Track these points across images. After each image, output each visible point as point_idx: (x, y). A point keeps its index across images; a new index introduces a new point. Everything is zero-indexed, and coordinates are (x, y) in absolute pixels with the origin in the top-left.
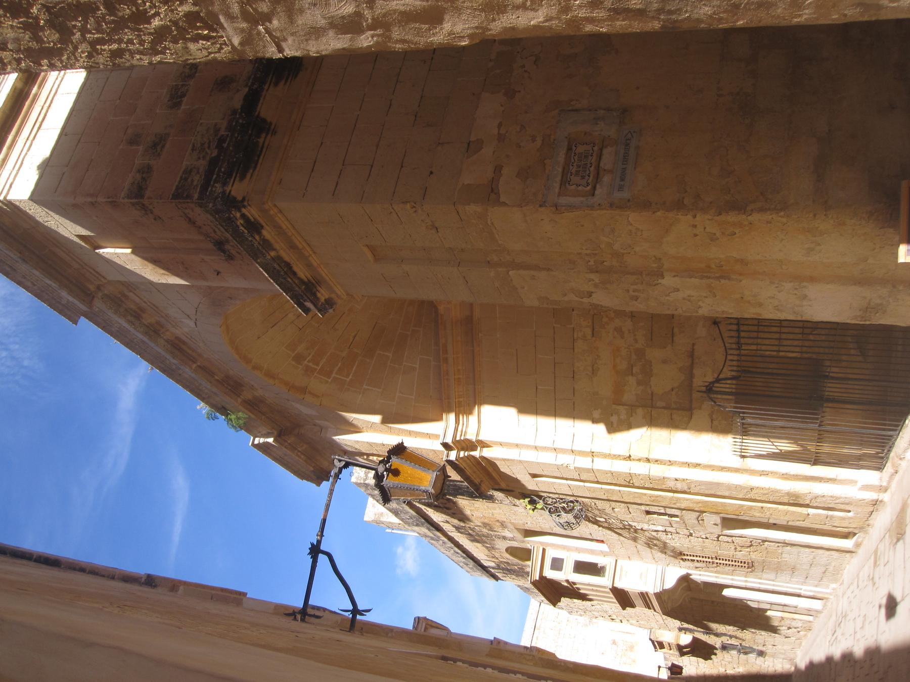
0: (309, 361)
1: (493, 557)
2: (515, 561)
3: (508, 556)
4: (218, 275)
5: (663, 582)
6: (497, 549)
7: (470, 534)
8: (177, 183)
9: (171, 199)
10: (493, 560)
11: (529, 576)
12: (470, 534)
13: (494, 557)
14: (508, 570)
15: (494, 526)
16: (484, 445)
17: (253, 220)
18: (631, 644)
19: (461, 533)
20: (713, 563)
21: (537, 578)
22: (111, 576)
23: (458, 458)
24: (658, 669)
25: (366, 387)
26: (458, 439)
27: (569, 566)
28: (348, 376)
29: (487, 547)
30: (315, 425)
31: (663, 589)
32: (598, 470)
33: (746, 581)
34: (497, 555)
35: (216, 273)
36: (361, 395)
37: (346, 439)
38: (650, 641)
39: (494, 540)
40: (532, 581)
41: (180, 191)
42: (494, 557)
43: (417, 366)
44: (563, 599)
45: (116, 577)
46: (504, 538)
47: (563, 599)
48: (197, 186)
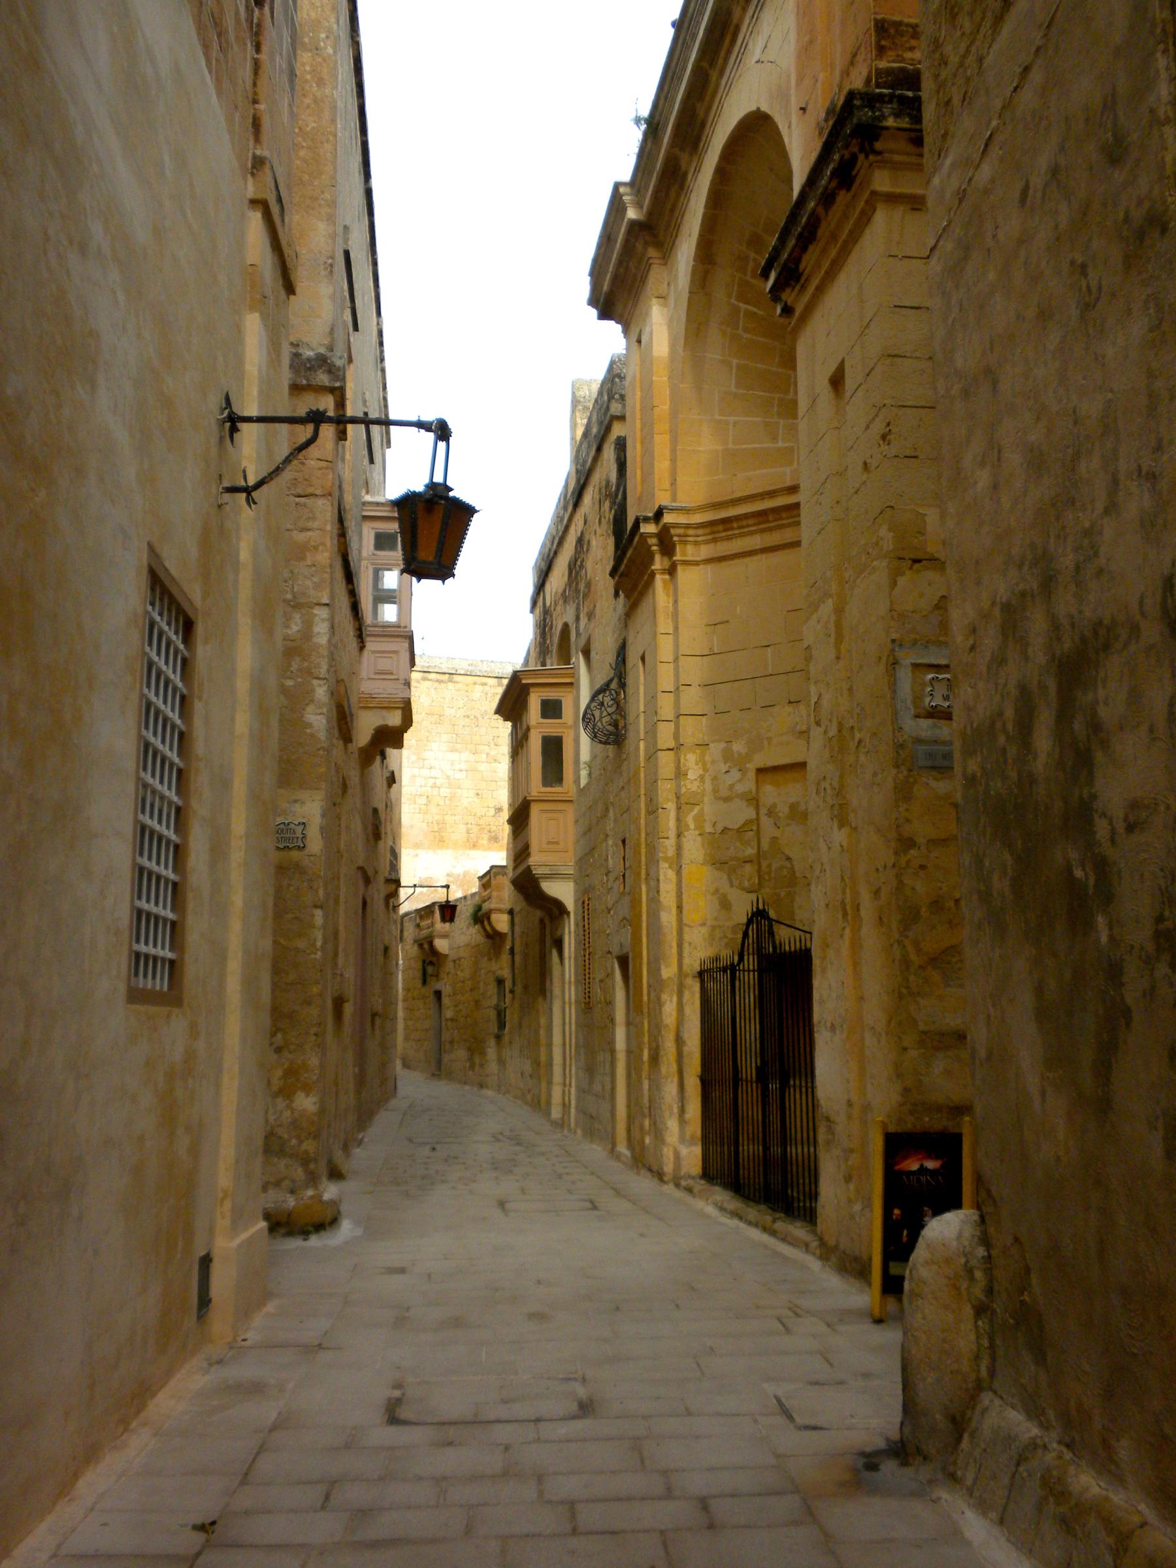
0: (755, 260)
1: (555, 602)
2: (556, 639)
3: (559, 627)
4: (802, 109)
5: (550, 877)
6: (565, 608)
7: (576, 560)
8: (906, 20)
9: (875, 19)
10: (553, 603)
11: (542, 666)
12: (576, 560)
13: (556, 605)
14: (544, 629)
15: (588, 600)
16: (671, 571)
17: (854, 173)
18: (501, 838)
19: (576, 548)
20: (585, 950)
21: (524, 682)
22: (256, 97)
23: (644, 537)
24: (444, 884)
25: (734, 364)
26: (673, 531)
27: (551, 727)
28: (746, 330)
29: (565, 591)
30: (669, 284)
31: (538, 878)
32: (657, 758)
33: (570, 1003)
34: (559, 608)
35: (803, 106)
36: (720, 358)
37: (1163, 117)
38: (488, 869)
39: (574, 602)
40: (518, 674)
41: (892, 31)
42: (556, 605)
43: (780, 444)
44: (509, 724)
45: (256, 106)
46: (578, 618)
47: (509, 724)
48: (903, 60)
